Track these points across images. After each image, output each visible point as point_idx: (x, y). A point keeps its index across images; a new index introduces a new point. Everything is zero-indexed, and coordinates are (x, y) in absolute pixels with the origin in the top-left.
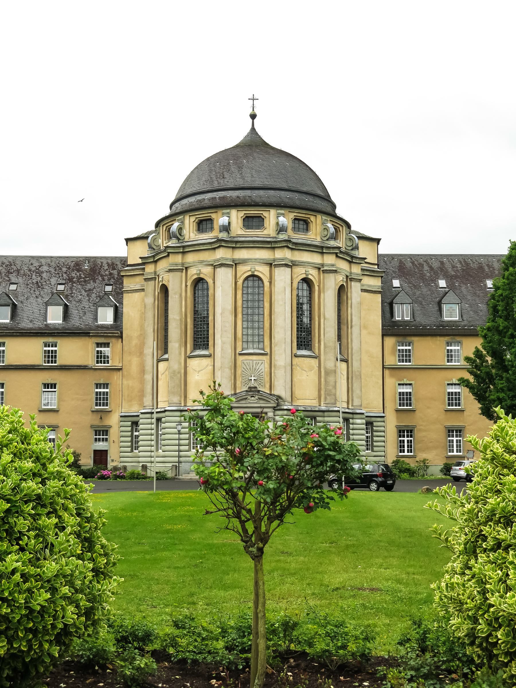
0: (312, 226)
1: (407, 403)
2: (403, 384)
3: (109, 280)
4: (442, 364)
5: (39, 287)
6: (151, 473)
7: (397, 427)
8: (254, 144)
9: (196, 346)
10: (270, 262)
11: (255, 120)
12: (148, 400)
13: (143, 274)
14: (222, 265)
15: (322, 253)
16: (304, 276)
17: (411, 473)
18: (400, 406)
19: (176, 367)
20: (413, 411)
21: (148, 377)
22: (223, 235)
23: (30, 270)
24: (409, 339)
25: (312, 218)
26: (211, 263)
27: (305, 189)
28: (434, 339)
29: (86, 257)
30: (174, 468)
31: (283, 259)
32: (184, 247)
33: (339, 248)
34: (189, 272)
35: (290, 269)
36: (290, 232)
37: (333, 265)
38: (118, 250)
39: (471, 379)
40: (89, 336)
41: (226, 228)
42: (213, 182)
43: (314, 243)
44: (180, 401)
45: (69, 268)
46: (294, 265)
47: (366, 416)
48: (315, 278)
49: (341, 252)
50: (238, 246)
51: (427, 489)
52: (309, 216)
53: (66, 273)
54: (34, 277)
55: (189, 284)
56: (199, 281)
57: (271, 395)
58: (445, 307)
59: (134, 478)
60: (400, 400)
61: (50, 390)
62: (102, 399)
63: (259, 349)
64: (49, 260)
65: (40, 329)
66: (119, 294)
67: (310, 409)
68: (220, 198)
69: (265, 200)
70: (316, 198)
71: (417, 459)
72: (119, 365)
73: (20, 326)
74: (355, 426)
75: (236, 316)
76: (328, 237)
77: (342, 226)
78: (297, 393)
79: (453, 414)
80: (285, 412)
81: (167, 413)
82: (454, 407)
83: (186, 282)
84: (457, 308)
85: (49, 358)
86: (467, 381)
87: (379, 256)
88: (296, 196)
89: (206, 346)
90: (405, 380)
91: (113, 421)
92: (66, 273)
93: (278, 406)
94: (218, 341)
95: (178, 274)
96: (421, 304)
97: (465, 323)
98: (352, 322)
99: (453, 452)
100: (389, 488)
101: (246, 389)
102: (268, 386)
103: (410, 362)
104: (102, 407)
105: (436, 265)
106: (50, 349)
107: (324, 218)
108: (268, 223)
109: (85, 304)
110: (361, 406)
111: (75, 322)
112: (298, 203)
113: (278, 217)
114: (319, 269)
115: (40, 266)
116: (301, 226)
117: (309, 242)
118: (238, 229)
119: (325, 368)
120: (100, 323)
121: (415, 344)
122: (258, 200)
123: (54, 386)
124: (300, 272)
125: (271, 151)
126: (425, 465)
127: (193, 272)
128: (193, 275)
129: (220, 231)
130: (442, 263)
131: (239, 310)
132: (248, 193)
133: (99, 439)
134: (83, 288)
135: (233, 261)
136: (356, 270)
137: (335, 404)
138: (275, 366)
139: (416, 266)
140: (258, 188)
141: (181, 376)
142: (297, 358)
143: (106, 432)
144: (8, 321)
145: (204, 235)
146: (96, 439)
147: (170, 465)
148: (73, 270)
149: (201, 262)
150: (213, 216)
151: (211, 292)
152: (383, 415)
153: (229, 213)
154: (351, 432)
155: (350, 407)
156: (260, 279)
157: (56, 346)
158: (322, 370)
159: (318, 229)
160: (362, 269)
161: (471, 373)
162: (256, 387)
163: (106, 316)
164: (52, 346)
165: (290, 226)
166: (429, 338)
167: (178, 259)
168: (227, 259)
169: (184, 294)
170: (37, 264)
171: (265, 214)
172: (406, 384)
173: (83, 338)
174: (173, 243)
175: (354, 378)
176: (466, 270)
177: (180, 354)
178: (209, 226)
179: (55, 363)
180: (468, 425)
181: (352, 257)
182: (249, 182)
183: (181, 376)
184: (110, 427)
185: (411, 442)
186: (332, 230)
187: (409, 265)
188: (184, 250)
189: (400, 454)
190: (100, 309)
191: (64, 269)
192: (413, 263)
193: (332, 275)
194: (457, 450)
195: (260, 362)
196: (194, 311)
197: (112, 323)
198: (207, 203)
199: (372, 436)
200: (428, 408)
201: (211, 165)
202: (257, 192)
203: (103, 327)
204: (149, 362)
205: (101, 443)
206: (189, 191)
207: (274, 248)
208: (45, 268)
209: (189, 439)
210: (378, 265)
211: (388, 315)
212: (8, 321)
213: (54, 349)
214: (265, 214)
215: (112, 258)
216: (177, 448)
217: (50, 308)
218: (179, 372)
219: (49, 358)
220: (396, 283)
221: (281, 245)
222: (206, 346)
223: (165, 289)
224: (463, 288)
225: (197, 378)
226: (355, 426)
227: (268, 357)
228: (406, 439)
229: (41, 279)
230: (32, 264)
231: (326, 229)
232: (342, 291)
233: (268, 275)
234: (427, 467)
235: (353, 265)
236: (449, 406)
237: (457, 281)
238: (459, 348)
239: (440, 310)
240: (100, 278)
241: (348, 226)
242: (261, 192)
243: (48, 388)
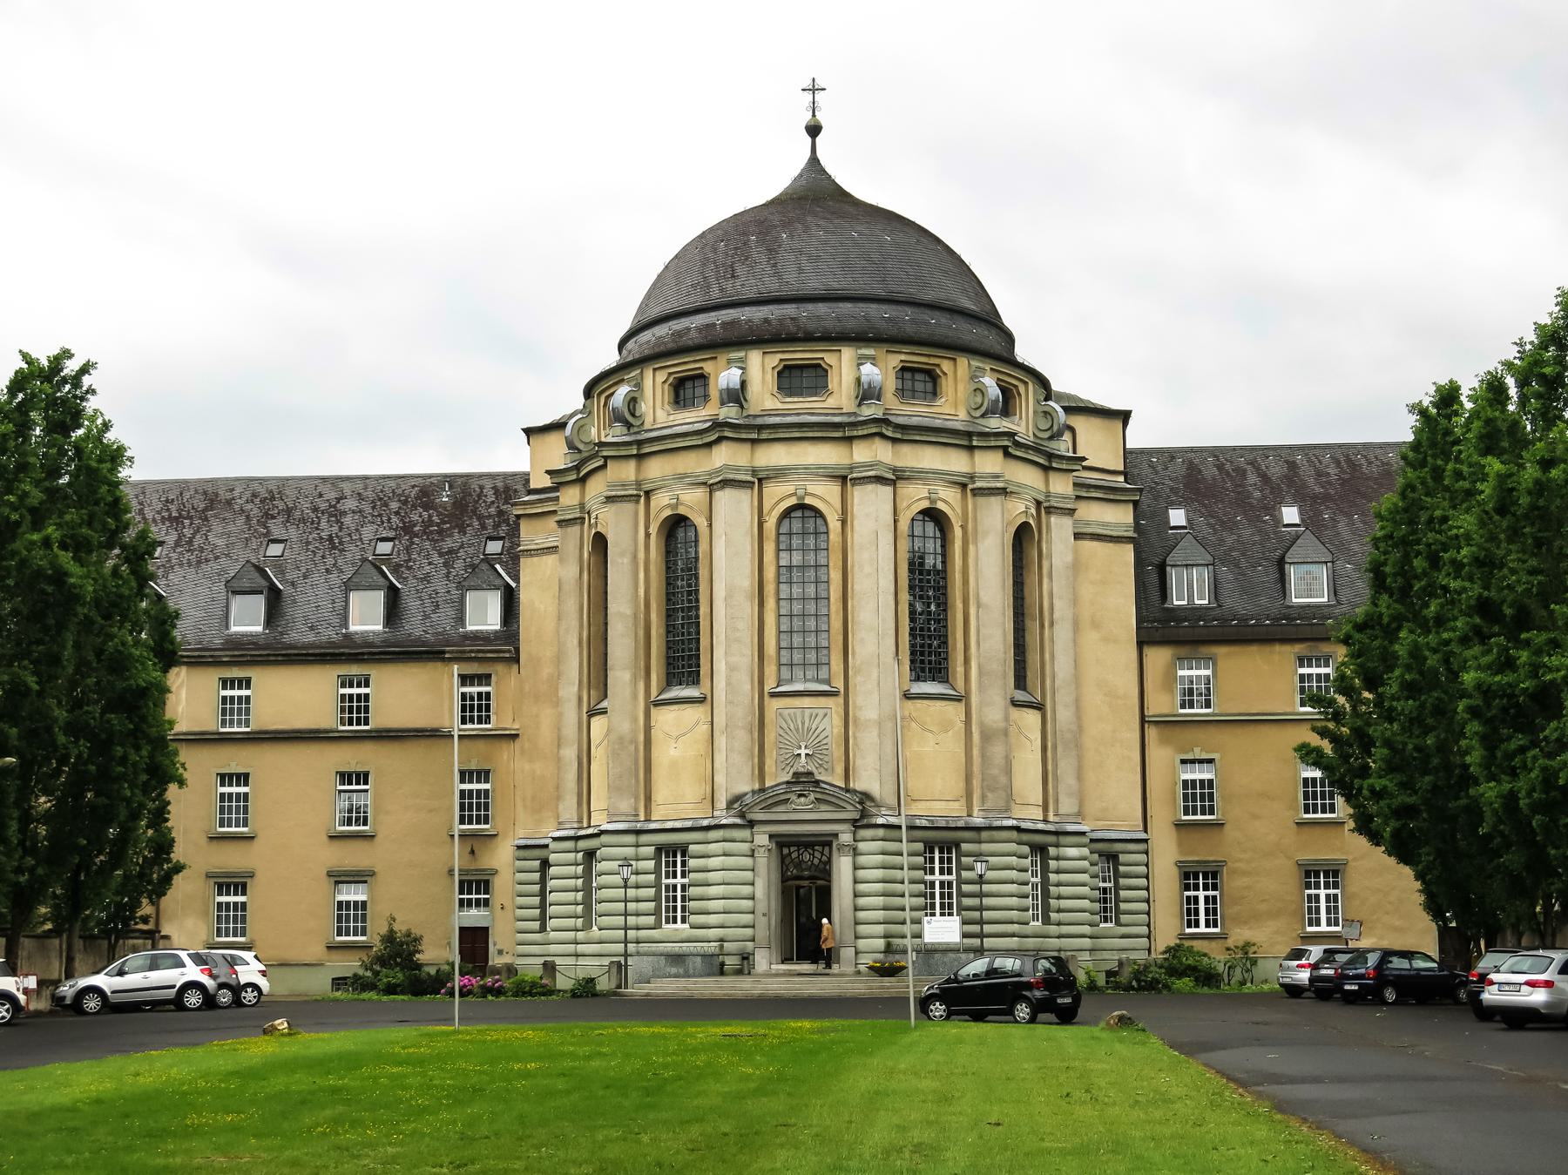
0: (946, 385)
1: (1323, 806)
2: (1193, 762)
3: (496, 526)
5: (334, 548)
6: (563, 983)
7: (1180, 864)
8: (816, 196)
10: (843, 472)
14: (726, 483)
15: (971, 449)
16: (925, 504)
17: (1208, 978)
19: (625, 727)
21: (570, 753)
22: (729, 413)
23: (315, 510)
25: (946, 366)
26: (702, 479)
27: (928, 296)
28: (1267, 649)
29: (446, 476)
30: (614, 970)
31: (871, 466)
32: (640, 443)
33: (1011, 435)
35: (889, 489)
36: (890, 400)
37: (996, 477)
39: (1327, 747)
40: (443, 660)
41: (736, 396)
42: (709, 287)
43: (950, 425)
44: (636, 809)
45: (405, 503)
46: (899, 478)
48: (953, 509)
49: (1018, 445)
50: (764, 436)
51: (1121, 1018)
53: (397, 513)
54: (324, 524)
55: (653, 530)
56: (676, 525)
57: (847, 791)
58: (1292, 572)
59: (524, 994)
61: (354, 787)
62: (475, 808)
63: (818, 681)
64: (359, 486)
65: (332, 644)
66: (513, 559)
67: (943, 824)
68: (723, 323)
69: (829, 324)
70: (956, 317)
71: (1230, 943)
73: (286, 639)
74: (1064, 864)
76: (983, 409)
77: (1026, 383)
78: (913, 784)
79: (1317, 831)
80: (881, 832)
81: (604, 839)
83: (647, 527)
84: (1323, 573)
85: (351, 712)
86: (1319, 751)
87: (1127, 453)
88: (907, 314)
89: (695, 679)
90: (1197, 750)
91: (501, 857)
92: (397, 513)
93: (863, 817)
95: (628, 507)
96: (1237, 566)
97: (1344, 608)
98: (1052, 613)
99: (1318, 924)
100: (1067, 1016)
101: (788, 778)
102: (840, 769)
104: (474, 826)
105: (1276, 470)
106: (355, 691)
107: (975, 363)
108: (836, 380)
109: (439, 584)
110: (1079, 814)
111: (414, 627)
112: (910, 330)
114: (964, 486)
115: (338, 500)
116: (919, 386)
117: (938, 423)
118: (765, 397)
120: (470, 628)
121: (1220, 663)
122: (811, 326)
123: (363, 777)
124: (915, 496)
125: (851, 209)
126: (1247, 956)
127: (662, 503)
129: (723, 404)
130: (1292, 466)
131: (770, 588)
132: (790, 310)
133: (470, 901)
134: (434, 548)
135: (754, 472)
136: (1061, 486)
139: (1228, 474)
140: (827, 300)
141: (636, 749)
143: (484, 885)
144: (260, 629)
145: (687, 415)
146: (461, 901)
147: (606, 961)
148: (414, 507)
149: (681, 477)
150: (708, 367)
151: (703, 547)
152: (1143, 836)
153: (742, 360)
154: (1053, 877)
155: (1051, 818)
156: (818, 513)
157: (367, 685)
158: (974, 728)
159: (962, 390)
160: (1075, 485)
161: (1323, 733)
162: (810, 774)
163: (484, 614)
164: (359, 686)
165: (891, 384)
166: (1254, 648)
167: (626, 471)
168: (737, 469)
169: (641, 555)
170: (332, 495)
171: (830, 359)
172: (1201, 761)
173: (430, 665)
174: (616, 434)
175: (1060, 749)
176: (1326, 478)
177: (635, 697)
178: (699, 391)
179: (366, 723)
180: (1355, 859)
181: (1051, 456)
182: (793, 282)
183: (636, 749)
184: (495, 872)
185: (1215, 902)
186: (994, 391)
187: (1210, 472)
188: (641, 449)
189: (1188, 931)
190: (469, 596)
191: (394, 505)
192: (1220, 467)
193: (995, 502)
194: (1207, 922)
195: (821, 712)
197: (498, 627)
198: (694, 338)
199: (1117, 887)
200: (1255, 817)
201: (708, 249)
202: (810, 306)
203: (476, 637)
205: (474, 911)
206: (655, 311)
208: (350, 504)
209: (657, 899)
210: (1124, 473)
211: (1155, 595)
212: (260, 629)
213: (363, 691)
214: (830, 359)
215: (506, 476)
216: (620, 920)
217: (354, 597)
218: (634, 741)
219: (351, 712)
220: (1177, 517)
222: (695, 679)
223: (600, 542)
224: (1342, 526)
225: (672, 752)
226: (1064, 864)
227: (841, 700)
228: (1201, 894)
229: (341, 529)
230: (321, 495)
231: (980, 391)
232: (1023, 538)
233: (838, 506)
234: (1254, 962)
235: (1053, 476)
236: (1307, 811)
237: (1327, 508)
238: (1208, 672)
239: (1282, 579)
240: (476, 523)
241: (1043, 382)
242: (822, 308)
243: (350, 783)
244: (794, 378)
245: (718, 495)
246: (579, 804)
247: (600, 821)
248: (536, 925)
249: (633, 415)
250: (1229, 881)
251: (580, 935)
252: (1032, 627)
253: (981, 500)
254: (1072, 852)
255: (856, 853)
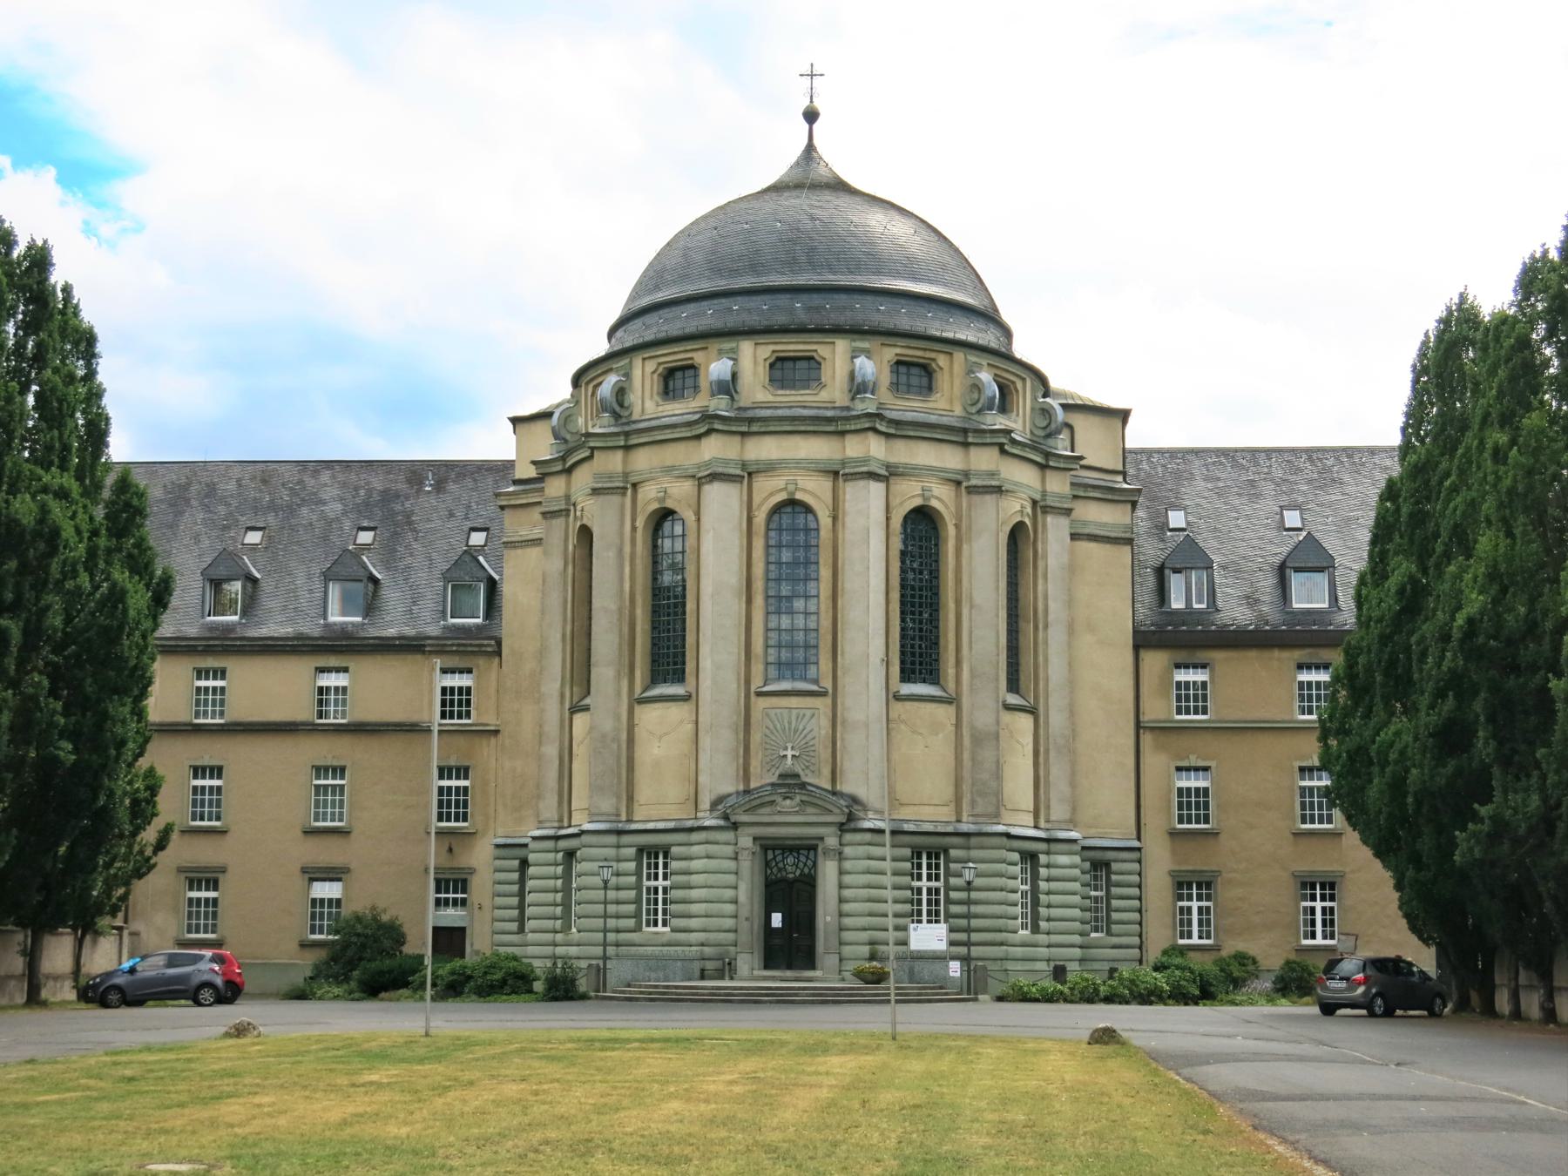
0: (942, 380)
2: (1188, 769)
4: (1287, 718)
7: (1173, 874)
8: (810, 178)
9: (656, 677)
10: (835, 468)
11: (815, 126)
12: (549, 807)
13: (539, 503)
14: (714, 477)
15: (966, 445)
16: (918, 502)
18: (1181, 821)
19: (608, 725)
20: (1213, 834)
21: (551, 751)
22: (720, 405)
24: (1203, 656)
25: (942, 360)
26: (691, 472)
28: (1266, 654)
30: (594, 971)
32: (627, 434)
33: (1008, 432)
34: (640, 496)
36: (884, 394)
37: (992, 474)
38: (499, 445)
40: (424, 652)
41: (728, 387)
43: (945, 421)
47: (1084, 848)
49: (1014, 442)
50: (755, 428)
52: (933, 355)
55: (640, 523)
56: (664, 516)
57: (834, 793)
60: (1180, 808)
62: (453, 805)
71: (1224, 953)
72: (491, 721)
74: (1054, 872)
75: (749, 601)
77: (1024, 380)
81: (585, 839)
82: (1317, 826)
83: (634, 520)
89: (679, 677)
91: (480, 857)
94: (706, 664)
95: (616, 499)
101: (774, 779)
102: (827, 771)
103: (1205, 713)
107: (973, 359)
113: (853, 357)
114: (959, 483)
116: (915, 381)
117: (933, 419)
118: (756, 389)
119: (972, 728)
127: (649, 497)
128: (649, 502)
131: (759, 585)
133: (447, 901)
135: (744, 465)
136: (1058, 485)
137: (997, 815)
138: (844, 722)
141: (619, 747)
142: (899, 705)
143: (462, 884)
149: (668, 470)
150: (698, 358)
152: (1136, 844)
153: (733, 351)
155: (1042, 824)
156: (808, 509)
160: (1072, 484)
165: (886, 378)
166: (1252, 654)
167: (613, 462)
168: (726, 462)
169: (627, 549)
171: (823, 351)
172: (1197, 769)
173: (410, 657)
175: (1052, 754)
177: (619, 694)
180: (1353, 872)
181: (1047, 455)
183: (619, 747)
184: (472, 871)
189: (1181, 942)
193: (989, 499)
195: (809, 713)
196: (654, 589)
199: (1109, 896)
204: (553, 712)
205: (451, 911)
207: (843, 433)
218: (616, 739)
221: (859, 427)
222: (679, 677)
223: (586, 534)
225: (656, 751)
226: (1054, 872)
227: (828, 700)
228: (1318, 905)
231: (977, 387)
232: (1017, 537)
233: (830, 502)
244: (785, 370)
245: (706, 488)
246: (560, 803)
247: (582, 822)
248: (514, 926)
249: (621, 405)
250: (1224, 892)
251: (559, 937)
252: (1027, 629)
253: (976, 498)
254: (1063, 859)
255: (841, 857)
